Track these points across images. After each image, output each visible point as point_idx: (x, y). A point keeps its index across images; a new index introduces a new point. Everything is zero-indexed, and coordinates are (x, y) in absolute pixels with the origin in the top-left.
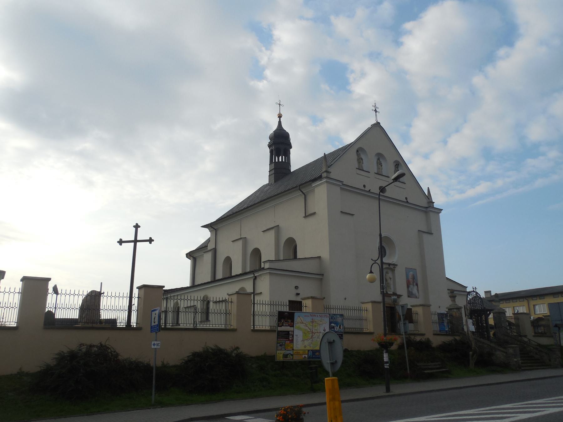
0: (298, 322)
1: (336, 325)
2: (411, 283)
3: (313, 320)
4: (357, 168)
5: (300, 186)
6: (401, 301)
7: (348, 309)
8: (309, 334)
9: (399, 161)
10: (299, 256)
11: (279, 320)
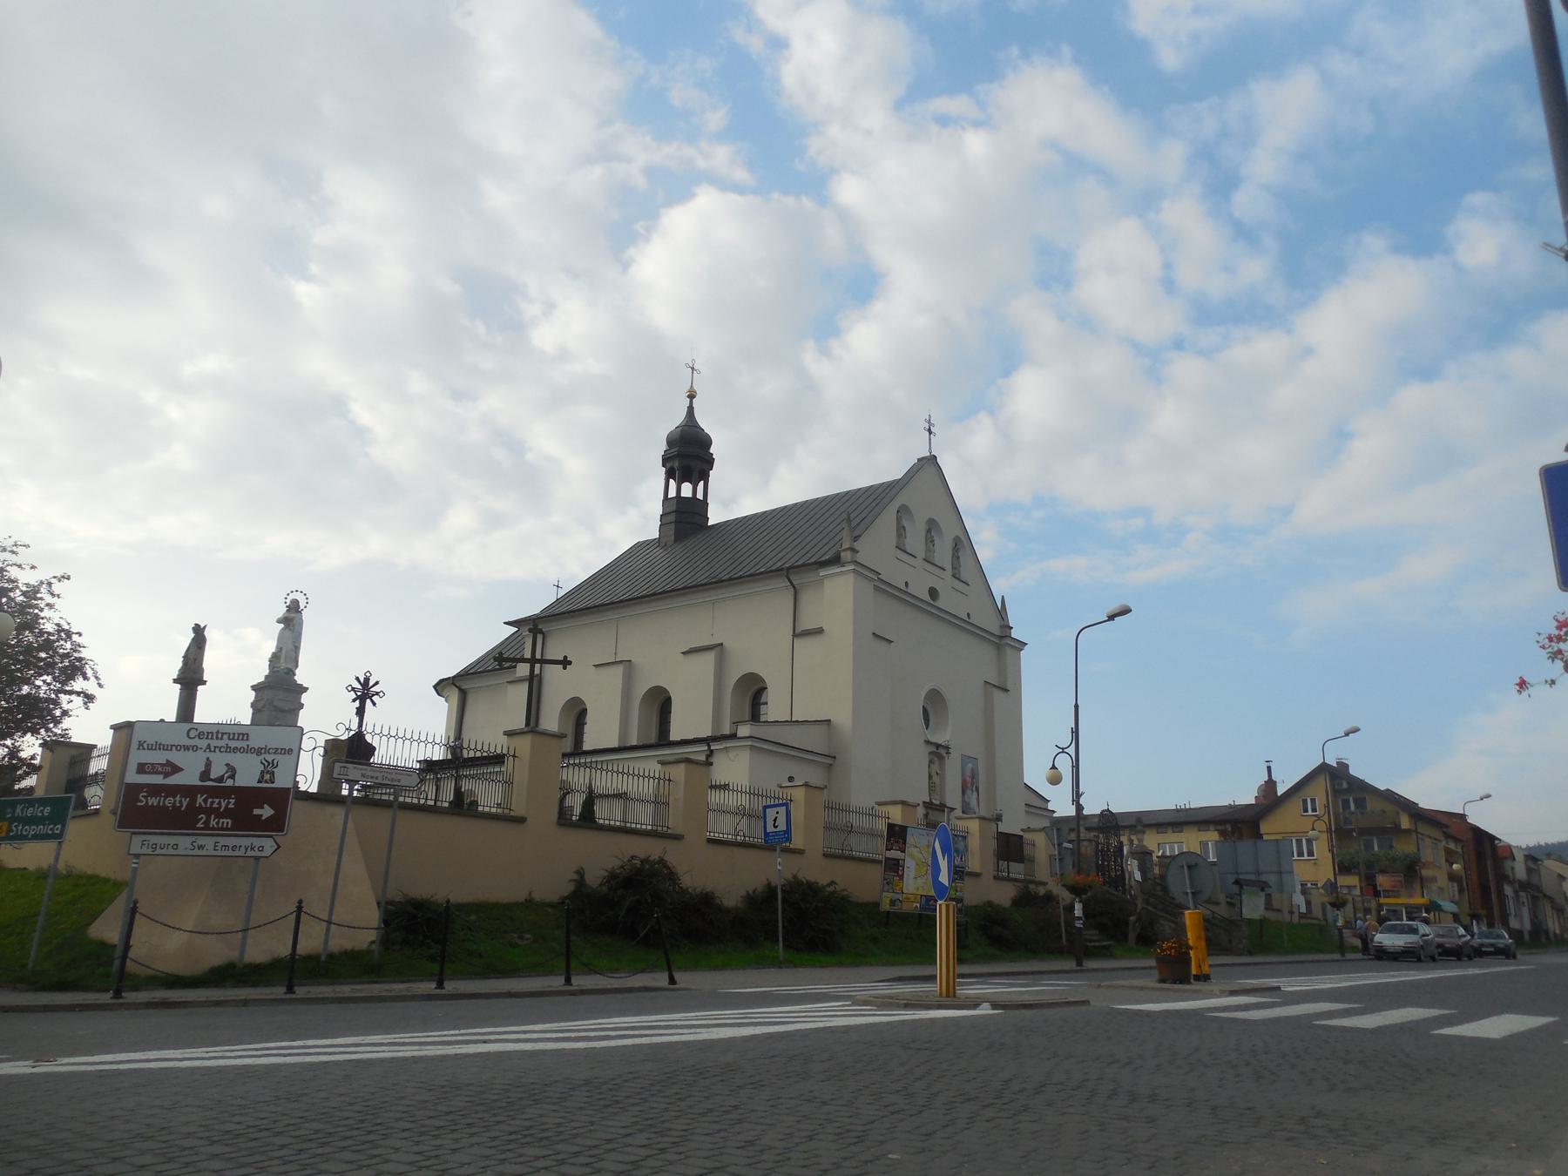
2: (969, 785)
5: (788, 569)
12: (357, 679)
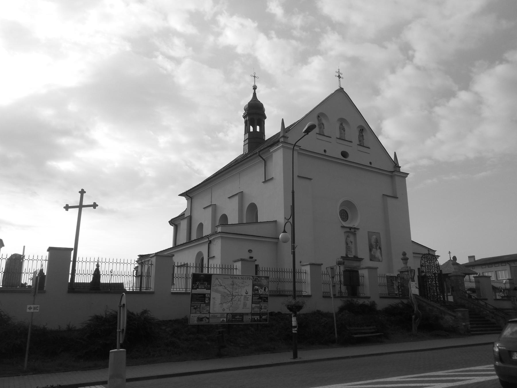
0: (215, 285)
1: (260, 288)
2: (374, 246)
3: (233, 282)
4: (359, 144)
6: (362, 264)
8: (229, 297)
9: (363, 125)
10: (258, 222)
11: (194, 282)
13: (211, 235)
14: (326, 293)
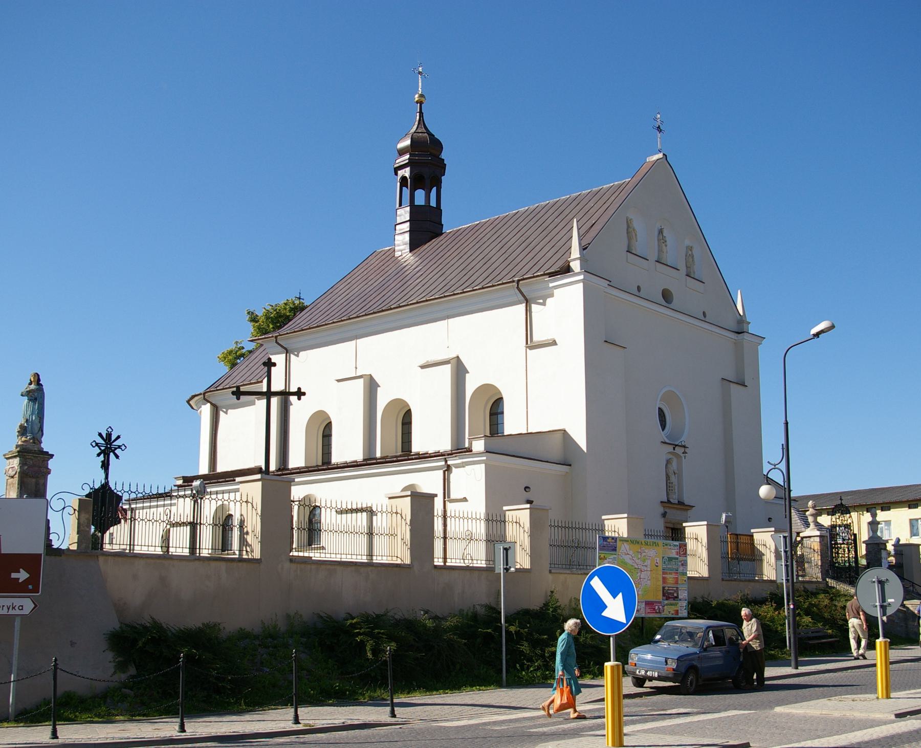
7: (463, 518)
12: (100, 435)
13: (450, 454)
14: (693, 572)
